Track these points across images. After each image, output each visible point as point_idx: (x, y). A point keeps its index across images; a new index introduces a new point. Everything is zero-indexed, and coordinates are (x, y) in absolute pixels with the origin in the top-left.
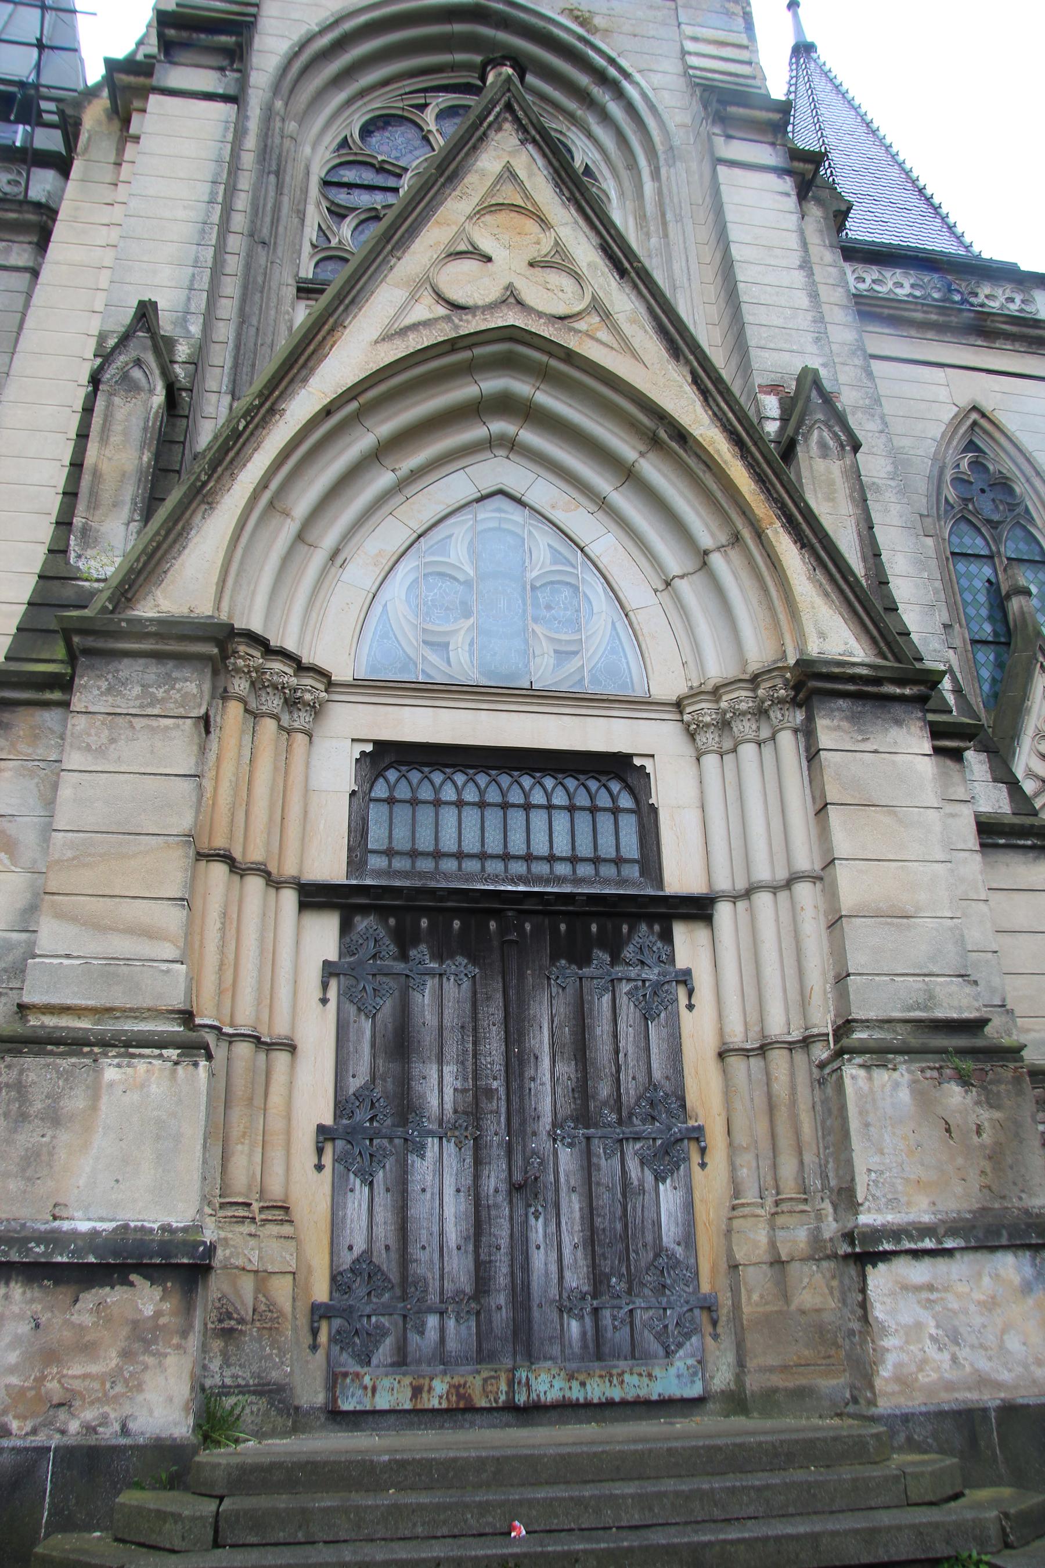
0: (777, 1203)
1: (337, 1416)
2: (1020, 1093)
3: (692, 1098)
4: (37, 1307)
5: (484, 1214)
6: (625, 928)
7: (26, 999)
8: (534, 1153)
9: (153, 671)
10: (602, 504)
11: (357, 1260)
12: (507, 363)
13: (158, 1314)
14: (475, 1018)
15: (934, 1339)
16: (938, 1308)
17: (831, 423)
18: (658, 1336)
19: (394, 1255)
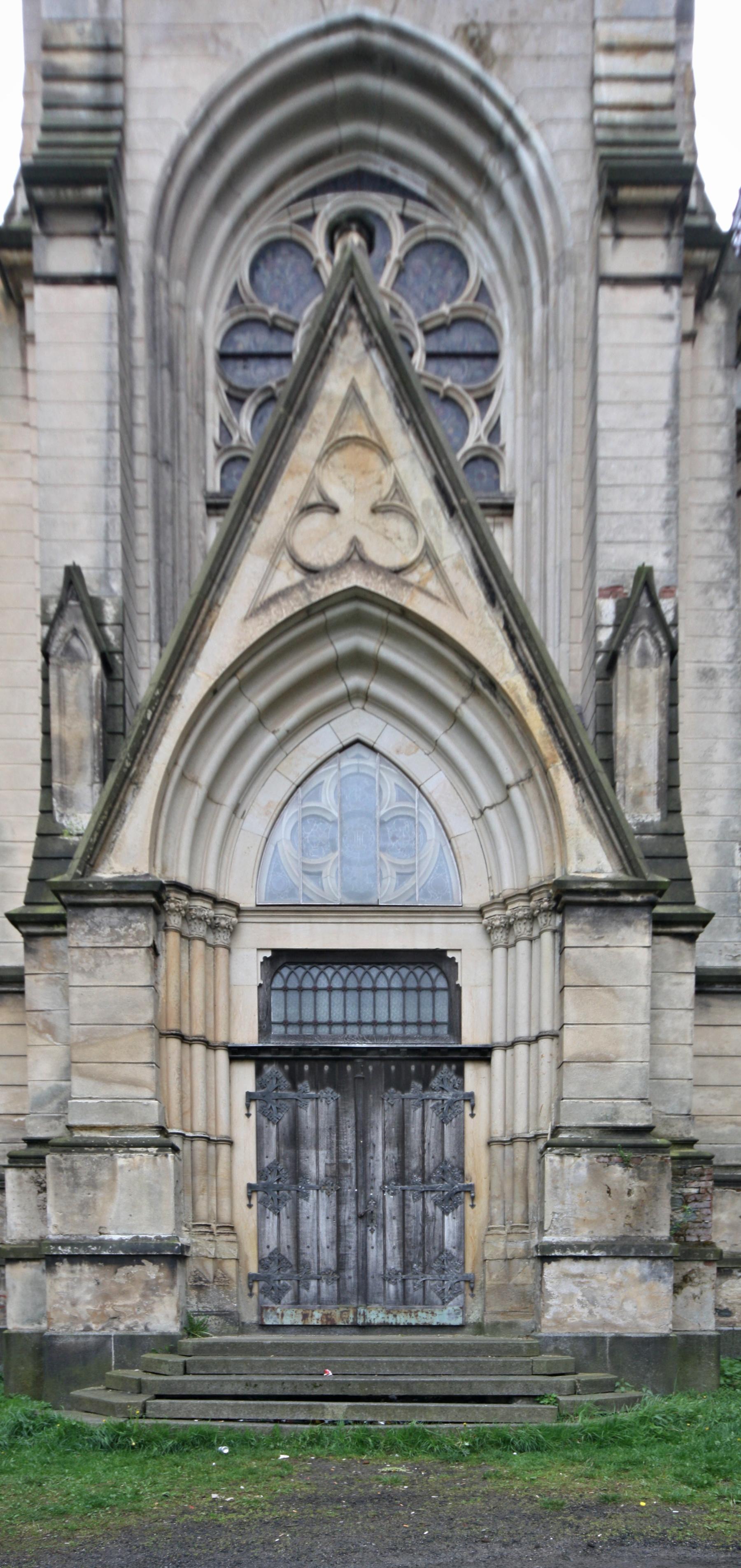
0: (512, 1227)
1: (263, 1327)
2: (662, 1171)
3: (469, 1168)
4: (97, 1275)
5: (342, 1230)
6: (433, 1068)
7: (71, 1123)
8: (372, 1198)
9: (115, 916)
10: (435, 746)
11: (272, 1253)
12: (357, 621)
13: (158, 1278)
14: (337, 1123)
15: (580, 1302)
16: (585, 1286)
17: (655, 628)
18: (439, 1294)
19: (292, 1251)
